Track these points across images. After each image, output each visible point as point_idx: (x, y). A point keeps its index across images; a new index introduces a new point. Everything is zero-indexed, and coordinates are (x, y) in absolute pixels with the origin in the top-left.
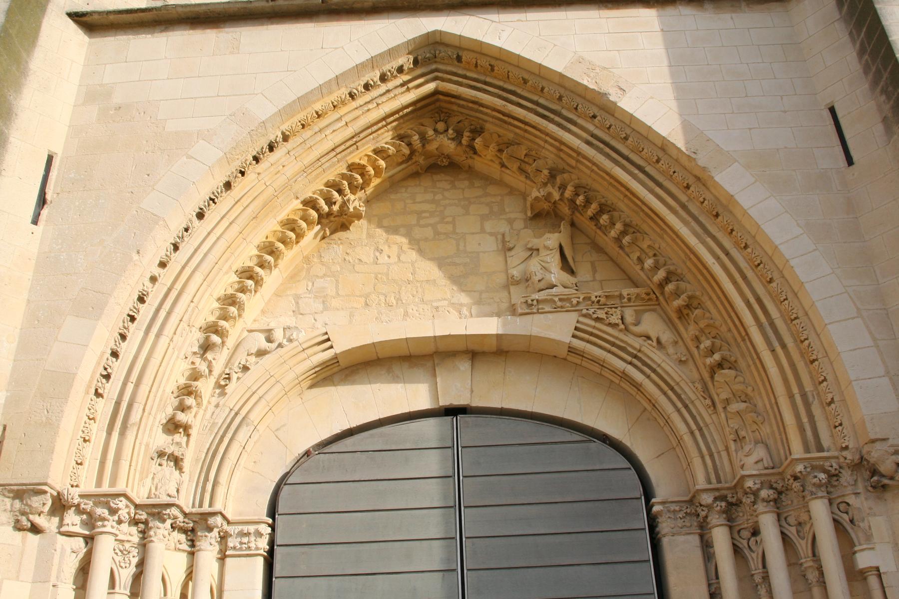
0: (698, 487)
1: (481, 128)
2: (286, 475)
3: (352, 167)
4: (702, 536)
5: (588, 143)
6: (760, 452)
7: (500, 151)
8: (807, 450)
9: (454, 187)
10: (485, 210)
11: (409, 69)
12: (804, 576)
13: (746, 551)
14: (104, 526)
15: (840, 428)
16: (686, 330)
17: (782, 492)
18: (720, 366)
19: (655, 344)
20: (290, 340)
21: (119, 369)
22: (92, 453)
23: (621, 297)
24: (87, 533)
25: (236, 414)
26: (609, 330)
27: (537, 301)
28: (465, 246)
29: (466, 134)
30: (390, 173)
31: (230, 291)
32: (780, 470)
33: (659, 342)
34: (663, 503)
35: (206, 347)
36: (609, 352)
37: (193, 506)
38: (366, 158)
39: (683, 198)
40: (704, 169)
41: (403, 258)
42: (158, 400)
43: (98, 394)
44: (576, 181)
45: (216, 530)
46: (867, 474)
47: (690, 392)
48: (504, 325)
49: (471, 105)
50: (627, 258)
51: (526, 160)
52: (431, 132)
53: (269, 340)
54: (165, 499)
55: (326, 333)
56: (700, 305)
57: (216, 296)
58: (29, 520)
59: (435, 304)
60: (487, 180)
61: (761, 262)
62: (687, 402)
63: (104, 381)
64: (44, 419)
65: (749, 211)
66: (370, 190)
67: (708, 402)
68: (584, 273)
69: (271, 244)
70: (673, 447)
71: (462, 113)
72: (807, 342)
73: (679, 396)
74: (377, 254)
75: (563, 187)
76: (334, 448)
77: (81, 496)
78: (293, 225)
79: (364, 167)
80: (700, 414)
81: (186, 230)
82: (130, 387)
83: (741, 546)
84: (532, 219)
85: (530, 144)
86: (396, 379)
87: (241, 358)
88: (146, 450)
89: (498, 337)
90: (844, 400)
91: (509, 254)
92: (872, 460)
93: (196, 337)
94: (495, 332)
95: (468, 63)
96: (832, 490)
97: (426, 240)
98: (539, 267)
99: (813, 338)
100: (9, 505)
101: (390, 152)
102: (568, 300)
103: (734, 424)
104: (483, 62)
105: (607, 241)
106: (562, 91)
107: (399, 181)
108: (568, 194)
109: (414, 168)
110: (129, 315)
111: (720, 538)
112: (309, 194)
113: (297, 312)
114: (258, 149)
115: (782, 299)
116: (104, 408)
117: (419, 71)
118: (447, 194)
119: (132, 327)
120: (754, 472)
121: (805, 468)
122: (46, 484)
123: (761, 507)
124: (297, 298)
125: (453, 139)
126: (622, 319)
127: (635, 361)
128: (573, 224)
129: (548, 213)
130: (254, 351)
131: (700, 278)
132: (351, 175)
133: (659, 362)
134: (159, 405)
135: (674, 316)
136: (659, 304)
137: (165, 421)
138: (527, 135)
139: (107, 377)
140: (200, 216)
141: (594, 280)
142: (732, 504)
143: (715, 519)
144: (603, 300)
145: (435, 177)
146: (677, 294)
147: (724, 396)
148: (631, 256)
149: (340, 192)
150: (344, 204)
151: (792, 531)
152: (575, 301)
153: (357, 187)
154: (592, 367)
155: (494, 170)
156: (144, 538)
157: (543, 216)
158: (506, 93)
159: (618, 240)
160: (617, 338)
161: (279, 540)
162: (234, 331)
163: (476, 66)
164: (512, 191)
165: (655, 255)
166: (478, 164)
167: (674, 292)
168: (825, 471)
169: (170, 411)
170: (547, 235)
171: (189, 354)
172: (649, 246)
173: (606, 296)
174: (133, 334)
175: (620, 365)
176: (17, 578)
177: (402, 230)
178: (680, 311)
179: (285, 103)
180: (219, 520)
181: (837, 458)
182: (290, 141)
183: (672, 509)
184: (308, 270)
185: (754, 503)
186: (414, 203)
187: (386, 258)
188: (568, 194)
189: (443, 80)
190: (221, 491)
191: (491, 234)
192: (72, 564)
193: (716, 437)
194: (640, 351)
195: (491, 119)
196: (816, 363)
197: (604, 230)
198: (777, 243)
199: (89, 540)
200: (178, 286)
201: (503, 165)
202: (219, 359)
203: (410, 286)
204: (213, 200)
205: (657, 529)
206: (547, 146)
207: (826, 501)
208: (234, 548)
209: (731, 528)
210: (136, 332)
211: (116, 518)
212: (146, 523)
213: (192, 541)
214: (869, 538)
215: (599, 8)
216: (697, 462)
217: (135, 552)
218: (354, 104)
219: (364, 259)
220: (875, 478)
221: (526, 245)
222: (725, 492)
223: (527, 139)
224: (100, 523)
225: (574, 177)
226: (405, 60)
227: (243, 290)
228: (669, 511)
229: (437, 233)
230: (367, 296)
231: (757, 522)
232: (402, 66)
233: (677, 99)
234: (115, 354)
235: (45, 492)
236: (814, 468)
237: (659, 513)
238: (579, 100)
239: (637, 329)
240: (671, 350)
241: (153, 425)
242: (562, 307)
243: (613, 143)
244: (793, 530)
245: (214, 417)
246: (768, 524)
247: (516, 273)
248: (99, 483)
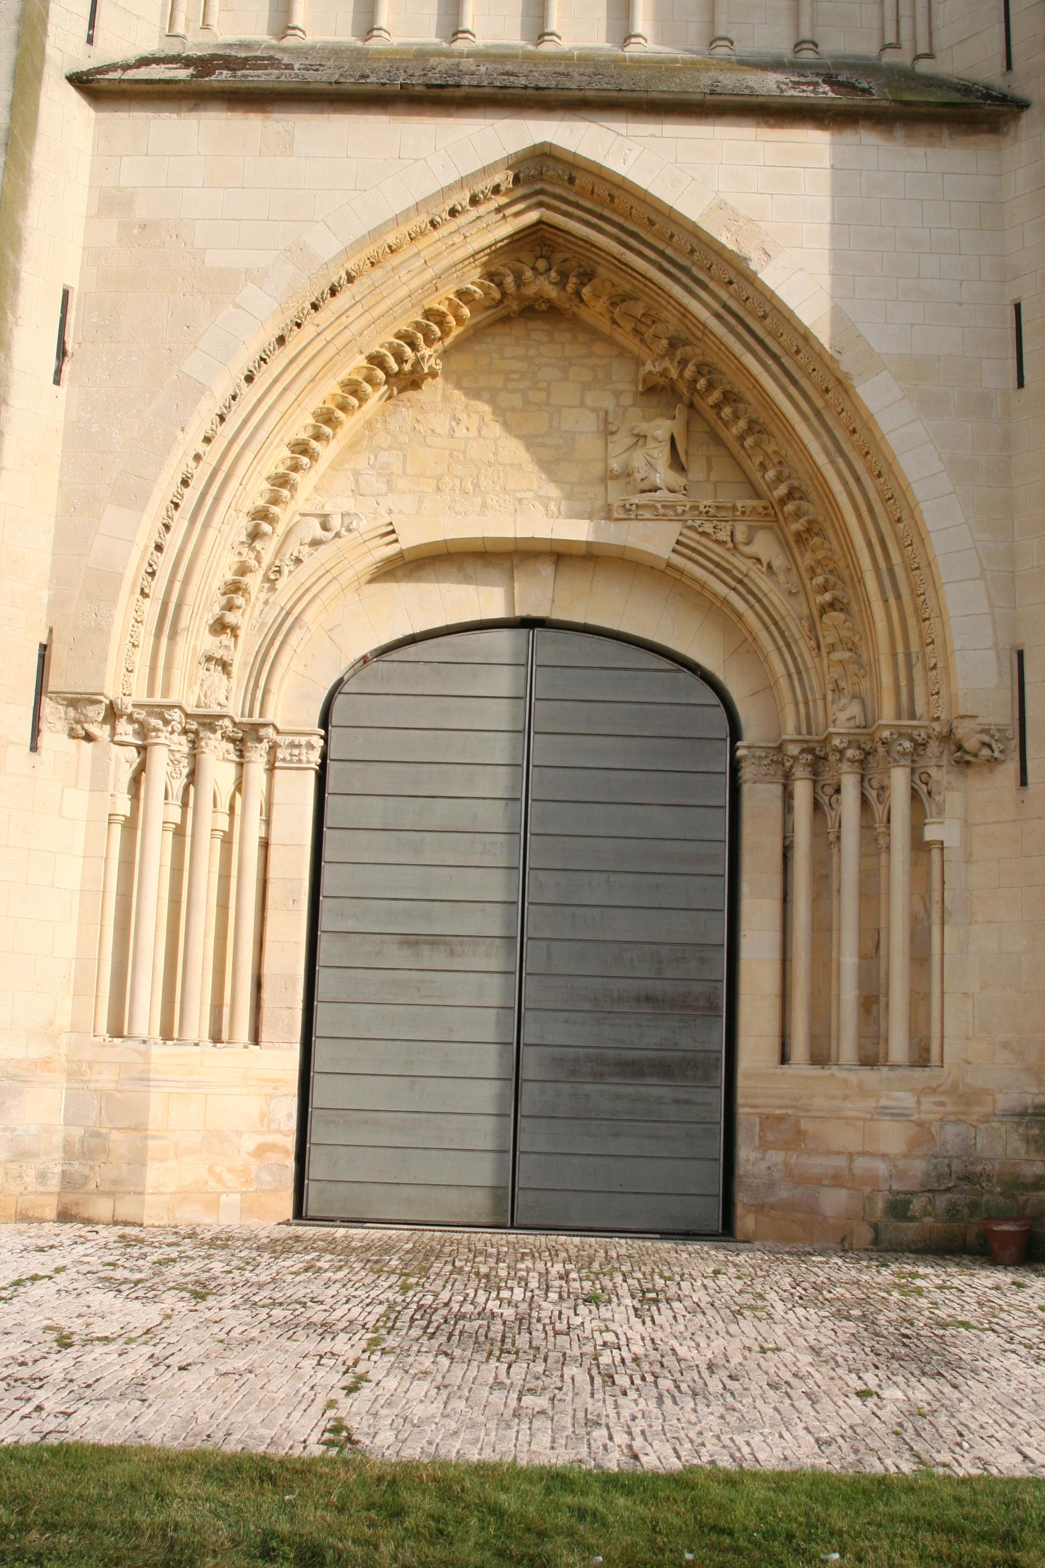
0: (785, 737)
1: (592, 271)
2: (340, 682)
3: (428, 314)
4: (785, 786)
5: (717, 316)
6: (855, 709)
7: (614, 304)
8: (898, 717)
9: (552, 340)
11: (507, 189)
12: (876, 840)
13: (826, 809)
14: (158, 737)
15: (936, 697)
16: (802, 557)
17: (868, 757)
18: (832, 605)
19: (764, 569)
20: (349, 530)
21: (164, 563)
22: (141, 659)
23: (734, 508)
24: (140, 743)
25: (288, 613)
27: (637, 506)
28: (559, 423)
29: (573, 280)
30: (475, 321)
31: (282, 470)
32: (871, 731)
33: (769, 566)
34: (749, 747)
35: (255, 535)
36: (712, 573)
37: (243, 715)
38: (447, 303)
39: (819, 403)
40: (847, 374)
41: (484, 432)
42: (204, 597)
43: (144, 594)
44: (700, 358)
45: (265, 741)
46: (953, 748)
47: (796, 629)
48: (597, 530)
49: (581, 243)
50: (748, 461)
51: (643, 320)
52: (529, 274)
53: (325, 528)
54: (216, 710)
55: (391, 524)
56: (820, 533)
57: (265, 474)
58: (83, 728)
59: (519, 495)
60: (595, 334)
62: (790, 640)
63: (150, 579)
64: (93, 623)
66: (448, 341)
67: (813, 643)
68: (697, 471)
69: (330, 412)
70: (767, 688)
71: (569, 249)
72: (922, 598)
73: (781, 633)
74: (454, 424)
75: (683, 363)
76: (394, 655)
77: (134, 706)
78: (356, 387)
79: (443, 315)
80: (801, 655)
81: (234, 398)
82: (177, 585)
83: (822, 802)
84: (643, 394)
85: (648, 300)
86: (467, 580)
87: (293, 548)
88: (194, 654)
89: (587, 543)
90: (946, 667)
91: (611, 439)
92: (958, 736)
93: (243, 524)
94: (584, 539)
95: (583, 188)
96: (917, 759)
97: (513, 410)
98: (644, 462)
99: (930, 593)
100: (62, 712)
101: (477, 296)
102: (673, 507)
103: (835, 673)
104: (602, 190)
106: (695, 243)
107: (485, 327)
109: (505, 312)
110: (172, 502)
111: (802, 791)
112: (375, 348)
113: (357, 492)
114: (317, 294)
115: (906, 544)
116: (151, 609)
117: (520, 192)
118: (543, 350)
119: (177, 515)
120: (842, 731)
121: (892, 734)
122: (102, 694)
123: (845, 766)
124: (357, 473)
125: (555, 284)
127: (739, 587)
128: (691, 406)
129: (663, 388)
130: (308, 540)
131: (826, 501)
132: (427, 325)
133: (766, 591)
134: (205, 603)
135: (791, 540)
136: (777, 521)
137: (212, 622)
138: (646, 290)
139: (152, 574)
140: (249, 379)
141: (708, 480)
142: (818, 760)
143: (800, 772)
144: (712, 511)
145: (532, 325)
146: (797, 515)
147: (830, 640)
149: (413, 346)
150: (417, 363)
151: (872, 795)
152: (680, 510)
153: (434, 340)
154: (692, 585)
155: (604, 325)
156: (194, 748)
157: (657, 392)
158: (627, 235)
159: (742, 438)
160: (723, 558)
161: (332, 754)
162: (284, 515)
163: (592, 192)
164: (623, 352)
165: (780, 463)
166: (584, 313)
167: (793, 511)
168: (912, 740)
169: (216, 610)
171: (236, 544)
172: (774, 452)
173: (717, 507)
174: (177, 523)
175: (722, 590)
176: (76, 787)
177: (486, 395)
178: (798, 536)
179: (352, 239)
180: (270, 731)
181: (927, 727)
182: (356, 282)
183: (758, 754)
184: (371, 438)
185: (840, 760)
186: (502, 358)
187: (464, 430)
189: (549, 207)
190: (272, 700)
191: (593, 409)
192: (126, 774)
193: (815, 683)
194: (746, 575)
195: (604, 263)
196: (927, 622)
198: (910, 480)
199: (142, 749)
200: (225, 467)
201: (614, 322)
202: (268, 548)
203: (490, 472)
204: (264, 360)
205: (740, 774)
206: (670, 308)
207: (908, 770)
208: (284, 760)
209: (815, 782)
210: (180, 522)
211: (169, 729)
212: (196, 733)
213: (241, 751)
214: (941, 812)
215: (758, 125)
216: (790, 709)
217: (185, 762)
218: (436, 235)
219: (438, 430)
220: (959, 754)
221: (633, 429)
222: (812, 745)
223: (647, 294)
224: (154, 734)
225: (698, 351)
226: (503, 177)
227: (295, 468)
228: (754, 757)
229: (527, 402)
230: (439, 478)
231: (840, 780)
232: (498, 186)
233: (833, 274)
234: (159, 548)
235: (100, 702)
236: (900, 735)
237: (743, 758)
238: (714, 258)
239: (747, 550)
240: (782, 578)
241: (200, 625)
242: (664, 515)
243: (749, 320)
244: (874, 793)
245: (263, 615)
246: (850, 784)
247: (615, 465)
248: (151, 693)
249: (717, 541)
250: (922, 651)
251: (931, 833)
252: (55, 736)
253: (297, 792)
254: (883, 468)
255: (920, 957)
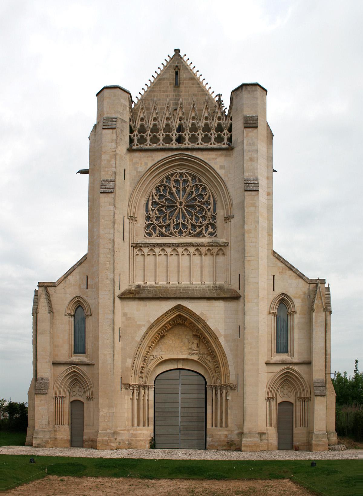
68: (200, 347)
111: (214, 391)
116: (133, 371)
167: (212, 354)
250: (227, 375)
251: (228, 398)
252: (123, 389)
253: (151, 393)
254: (222, 350)
255: (227, 414)
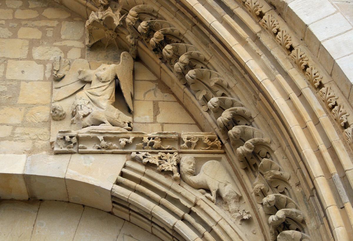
10: (37, 35)
19: (213, 198)
23: (179, 140)
26: (162, 178)
27: (78, 138)
33: (219, 195)
39: (256, 28)
61: (336, 104)
65: (323, 44)
68: (143, 113)
75: (124, 12)
105: (171, 77)
108: (129, 19)
126: (178, 165)
127: (188, 217)
128: (137, 59)
133: (217, 219)
148: (197, 95)
152: (123, 142)
159: (182, 74)
160: (170, 188)
165: (223, 95)
170: (104, 66)
173: (162, 139)
175: (170, 219)
188: (129, 19)
191: (39, 62)
194: (195, 205)
197: (169, 61)
239: (194, 179)
242: (107, 148)
249: (163, 172)
